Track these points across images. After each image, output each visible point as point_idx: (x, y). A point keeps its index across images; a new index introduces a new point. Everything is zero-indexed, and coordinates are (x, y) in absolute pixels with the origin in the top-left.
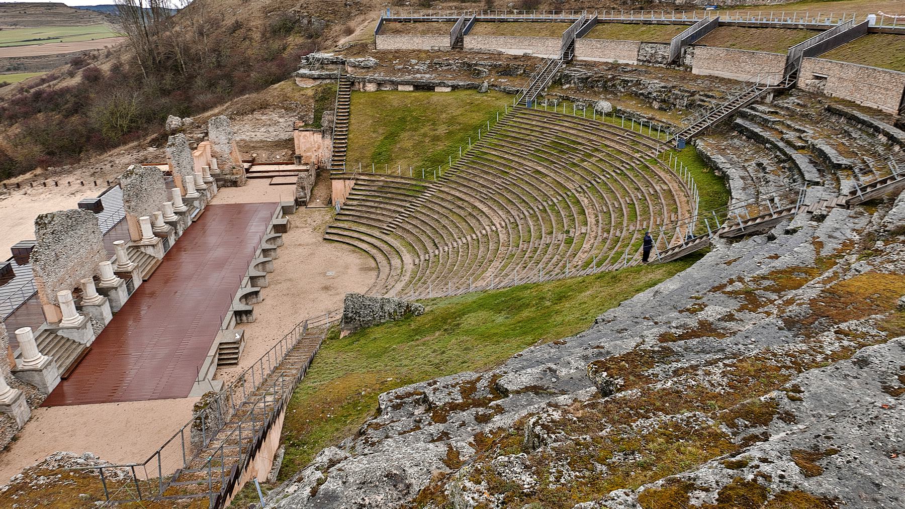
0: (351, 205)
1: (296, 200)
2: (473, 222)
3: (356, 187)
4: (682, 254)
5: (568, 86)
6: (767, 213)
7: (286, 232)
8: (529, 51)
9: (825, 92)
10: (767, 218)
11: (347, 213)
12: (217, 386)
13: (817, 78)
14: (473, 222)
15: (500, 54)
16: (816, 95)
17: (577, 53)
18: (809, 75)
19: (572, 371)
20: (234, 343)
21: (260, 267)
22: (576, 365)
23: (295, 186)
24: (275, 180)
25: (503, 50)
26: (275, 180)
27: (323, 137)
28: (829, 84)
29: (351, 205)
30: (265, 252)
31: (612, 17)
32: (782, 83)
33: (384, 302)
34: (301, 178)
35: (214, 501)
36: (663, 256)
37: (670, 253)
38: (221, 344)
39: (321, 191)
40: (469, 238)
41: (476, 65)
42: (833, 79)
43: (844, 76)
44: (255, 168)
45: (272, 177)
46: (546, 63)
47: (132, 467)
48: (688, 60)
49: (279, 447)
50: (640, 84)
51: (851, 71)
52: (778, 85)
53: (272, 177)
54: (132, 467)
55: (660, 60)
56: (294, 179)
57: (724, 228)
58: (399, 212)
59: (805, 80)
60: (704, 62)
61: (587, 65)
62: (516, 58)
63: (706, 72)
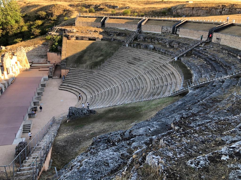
0: (65, 85)
1: (49, 76)
2: (109, 83)
3: (70, 72)
4: (175, 95)
5: (139, 40)
6: (206, 80)
7: (45, 87)
8: (127, 28)
9: (220, 43)
10: (206, 82)
11: (70, 75)
12: (24, 140)
13: (217, 39)
14: (109, 83)
15: (117, 29)
16: (219, 45)
17: (142, 29)
18: (215, 38)
19: (155, 129)
20: (29, 125)
21: (37, 99)
22: (156, 127)
23: (48, 71)
24: (41, 69)
25: (118, 28)
26: (41, 69)
27: (58, 55)
28: (222, 41)
29: (65, 85)
30: (39, 94)
31: (153, 18)
32: (207, 40)
33: (82, 110)
34: (50, 69)
35: (117, 19)
36: (173, 94)
37: (175, 93)
38: (24, 125)
39: (57, 72)
40: (109, 89)
41: (109, 32)
42: (223, 39)
43: (226, 39)
44: (33, 65)
45: (39, 68)
46: (132, 32)
47: (5, 167)
48: (178, 33)
49: (51, 159)
50: (162, 40)
51: (228, 37)
52: (206, 41)
53: (39, 68)
54: (5, 167)
55: (169, 32)
56: (48, 69)
57: (192, 85)
58: (85, 80)
59: (214, 40)
60: (182, 33)
61: (145, 33)
62: (122, 30)
63: (184, 36)
